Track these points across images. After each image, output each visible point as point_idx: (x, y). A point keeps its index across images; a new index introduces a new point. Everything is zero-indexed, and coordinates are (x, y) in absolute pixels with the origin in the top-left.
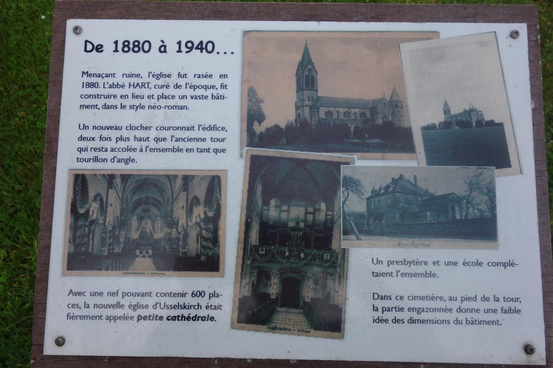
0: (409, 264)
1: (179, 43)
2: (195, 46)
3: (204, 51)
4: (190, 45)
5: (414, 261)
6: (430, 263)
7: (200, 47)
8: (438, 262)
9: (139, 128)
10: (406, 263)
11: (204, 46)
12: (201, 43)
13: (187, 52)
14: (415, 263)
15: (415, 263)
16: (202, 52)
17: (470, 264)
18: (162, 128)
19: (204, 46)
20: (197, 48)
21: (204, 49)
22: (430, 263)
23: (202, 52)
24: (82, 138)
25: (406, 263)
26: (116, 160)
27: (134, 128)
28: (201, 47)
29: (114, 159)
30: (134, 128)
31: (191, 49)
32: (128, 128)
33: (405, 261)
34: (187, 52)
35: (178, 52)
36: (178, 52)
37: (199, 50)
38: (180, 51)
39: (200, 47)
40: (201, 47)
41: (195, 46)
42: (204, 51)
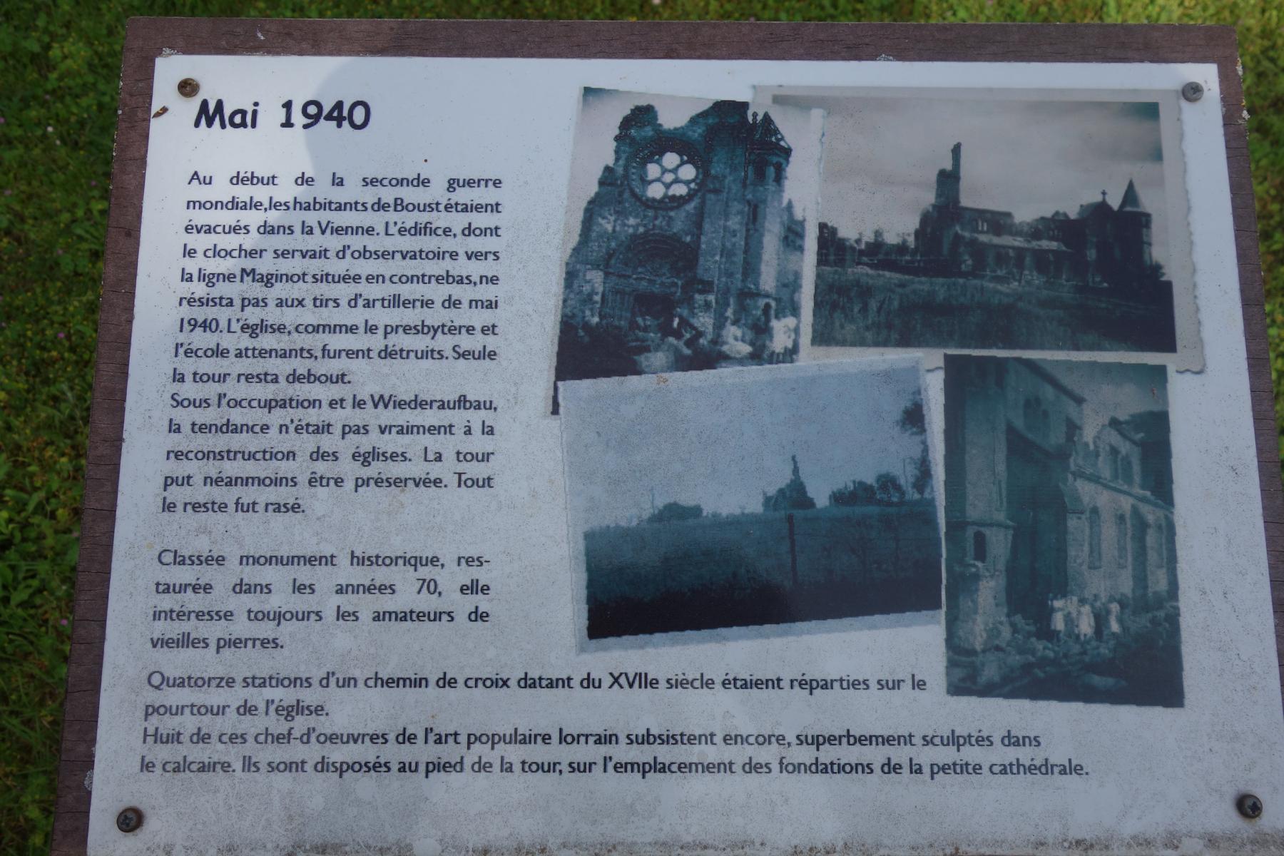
0: (432, 333)
1: (288, 105)
2: (325, 112)
3: (346, 123)
4: (312, 110)
5: (443, 326)
6: (366, 616)
7: (335, 114)
8: (494, 326)
9: (235, 254)
10: (426, 330)
11: (345, 113)
12: (339, 105)
13: (306, 127)
14: (446, 330)
15: (446, 330)
16: (339, 126)
17: (200, 353)
18: (404, 279)
19: (345, 113)
20: (329, 117)
21: (344, 119)
22: (366, 616)
23: (339, 126)
24: (492, 305)
25: (426, 330)
26: (361, 302)
27: (223, 253)
28: (338, 115)
29: (355, 299)
30: (223, 253)
31: (316, 119)
32: (210, 253)
33: (423, 326)
34: (306, 127)
35: (283, 125)
36: (283, 125)
37: (334, 123)
38: (288, 124)
39: (335, 114)
40: (338, 115)
41: (325, 112)
42: (346, 123)
